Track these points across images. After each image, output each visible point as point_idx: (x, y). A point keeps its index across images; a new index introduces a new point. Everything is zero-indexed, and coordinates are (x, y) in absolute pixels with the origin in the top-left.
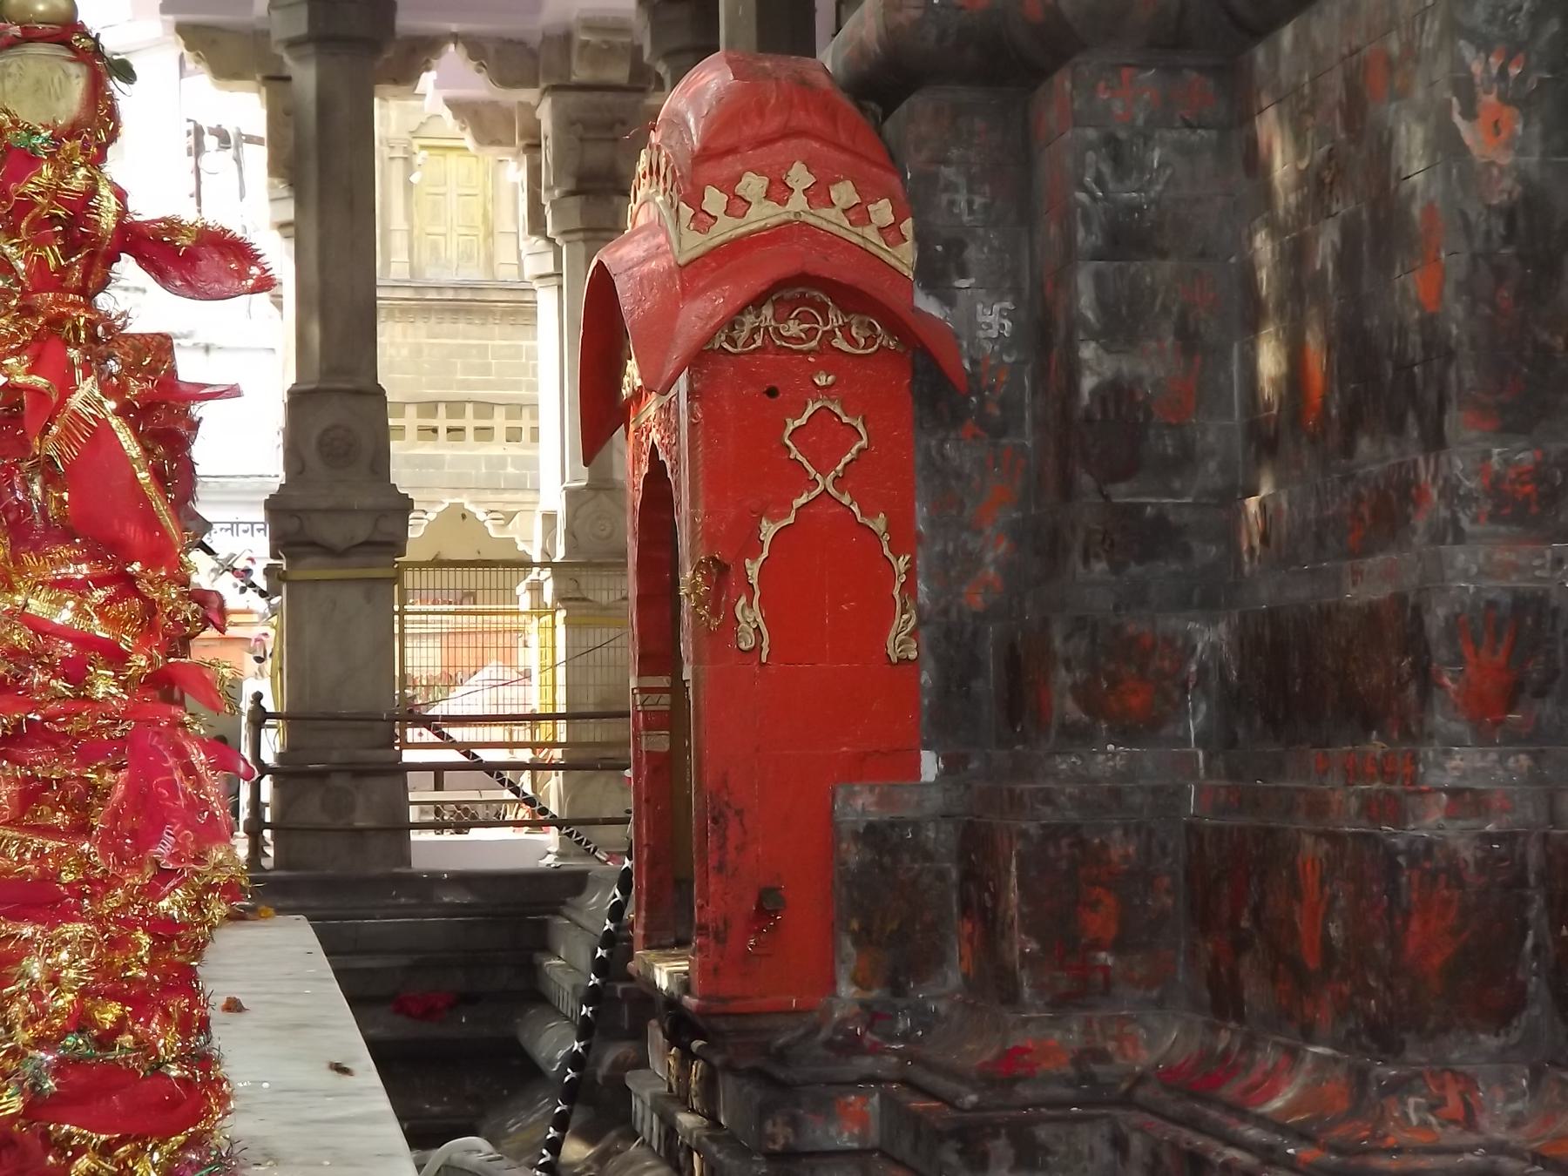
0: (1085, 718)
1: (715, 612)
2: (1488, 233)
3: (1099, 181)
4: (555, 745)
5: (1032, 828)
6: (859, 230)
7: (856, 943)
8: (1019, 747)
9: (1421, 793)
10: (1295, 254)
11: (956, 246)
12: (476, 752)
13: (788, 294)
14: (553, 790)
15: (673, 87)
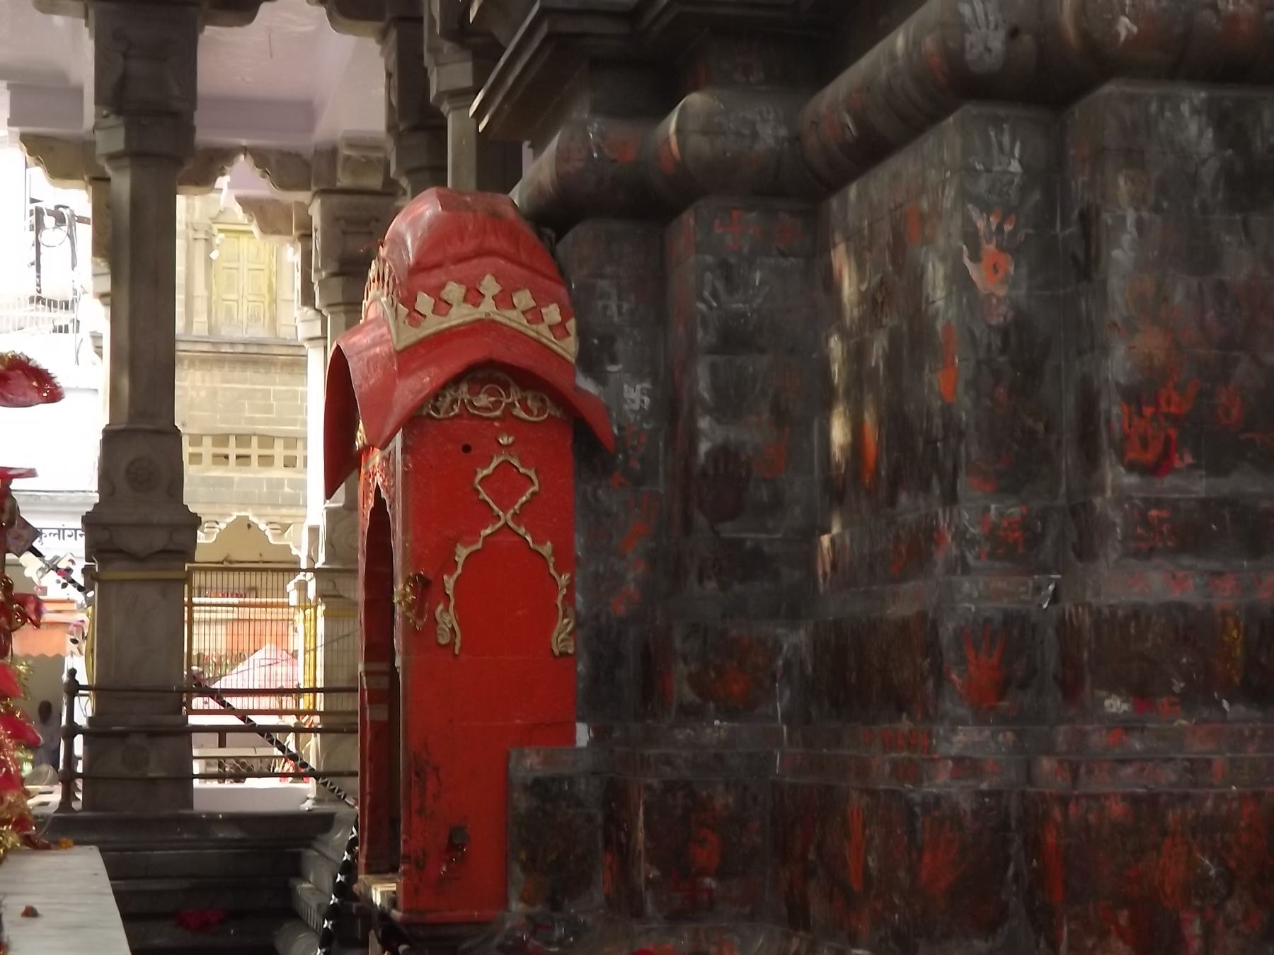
0: (698, 700)
1: (420, 615)
2: (989, 346)
3: (715, 295)
4: (313, 712)
5: (655, 783)
6: (534, 327)
7: (524, 868)
8: (649, 721)
9: (933, 760)
10: (857, 354)
11: (608, 341)
12: (251, 717)
13: (480, 375)
14: (312, 747)
15: (413, 197)
